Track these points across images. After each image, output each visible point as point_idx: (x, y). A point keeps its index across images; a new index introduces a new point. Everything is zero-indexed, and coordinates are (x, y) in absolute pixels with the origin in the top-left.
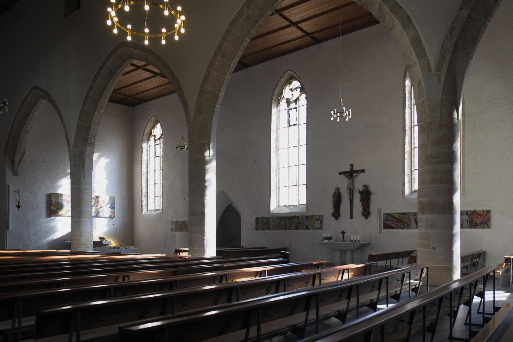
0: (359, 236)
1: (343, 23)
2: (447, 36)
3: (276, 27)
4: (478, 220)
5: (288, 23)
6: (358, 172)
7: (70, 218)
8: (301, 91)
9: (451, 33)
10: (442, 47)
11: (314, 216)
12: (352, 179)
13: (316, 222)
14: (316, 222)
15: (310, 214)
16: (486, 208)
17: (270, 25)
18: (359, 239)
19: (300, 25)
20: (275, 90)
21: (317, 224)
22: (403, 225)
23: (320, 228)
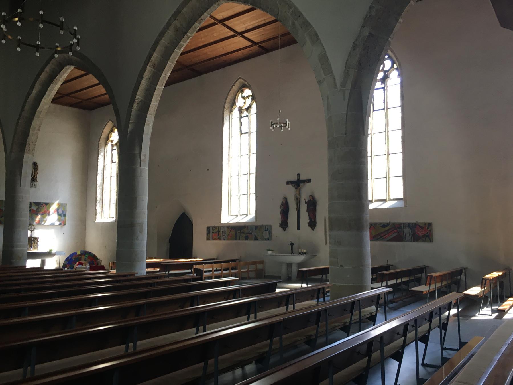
1: (282, 35)
2: (350, 53)
3: (222, 37)
4: (420, 233)
5: (233, 33)
6: (304, 181)
7: (401, 177)
8: (252, 99)
9: (354, 50)
10: (346, 63)
11: (262, 226)
12: (298, 189)
15: (259, 224)
16: (428, 221)
17: (215, 35)
19: (245, 35)
20: (227, 98)
21: (266, 235)
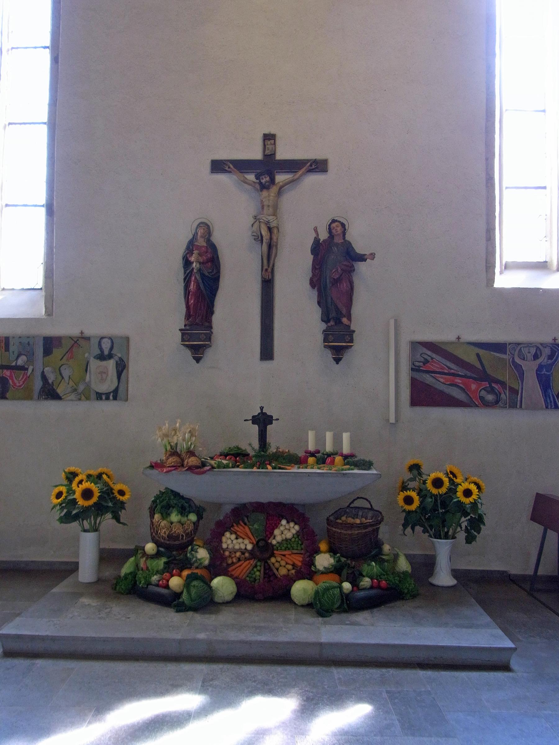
0: (346, 436)
6: (293, 166)
13: (94, 364)
14: (94, 364)
15: (64, 328)
18: (346, 450)
21: (103, 376)
22: (491, 391)
23: (114, 395)
